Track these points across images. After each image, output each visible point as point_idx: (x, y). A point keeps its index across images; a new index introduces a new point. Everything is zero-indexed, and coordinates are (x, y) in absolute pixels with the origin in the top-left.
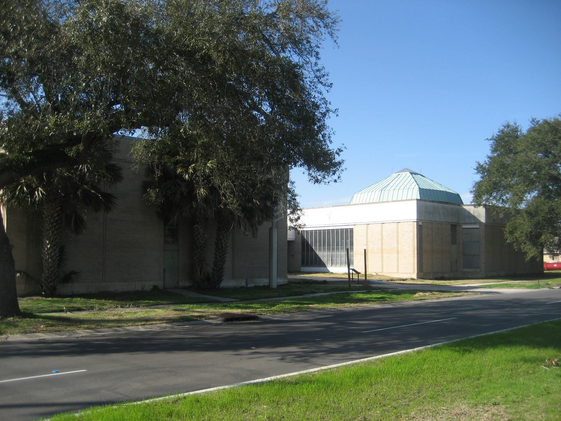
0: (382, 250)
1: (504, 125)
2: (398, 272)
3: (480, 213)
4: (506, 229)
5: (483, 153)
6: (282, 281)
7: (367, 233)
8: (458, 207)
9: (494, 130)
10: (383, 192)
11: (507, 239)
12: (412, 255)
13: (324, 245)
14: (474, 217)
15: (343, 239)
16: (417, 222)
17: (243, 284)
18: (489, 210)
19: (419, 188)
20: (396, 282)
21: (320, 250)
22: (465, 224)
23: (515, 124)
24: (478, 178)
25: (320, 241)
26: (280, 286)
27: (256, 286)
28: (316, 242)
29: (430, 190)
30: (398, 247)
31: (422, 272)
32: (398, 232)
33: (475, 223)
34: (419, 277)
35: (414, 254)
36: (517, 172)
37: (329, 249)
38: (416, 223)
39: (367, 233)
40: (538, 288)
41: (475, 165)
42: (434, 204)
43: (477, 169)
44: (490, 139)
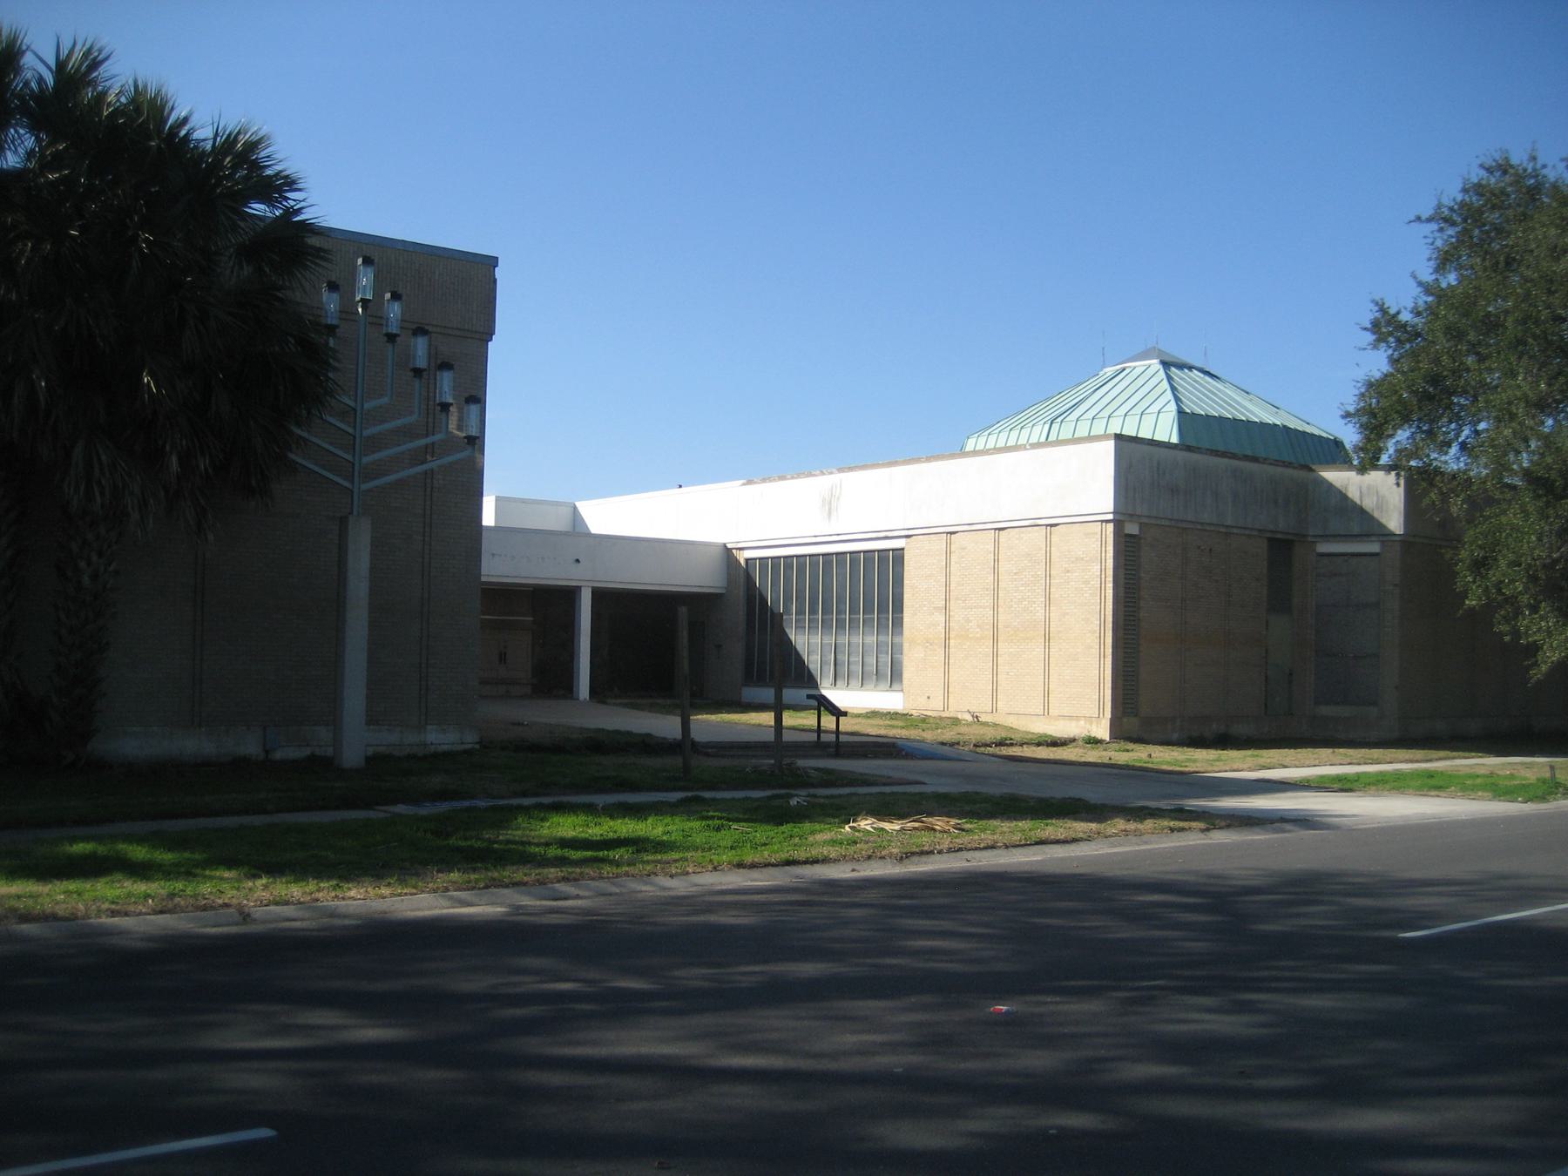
0: (995, 627)
1: (1489, 162)
2: (1046, 712)
3: (1380, 494)
4: (1464, 554)
5: (1405, 272)
6: (389, 739)
7: (948, 565)
8: (1302, 474)
9: (1449, 176)
10: (1056, 426)
11: (1464, 595)
12: (1095, 651)
13: (813, 611)
14: (1361, 511)
15: (867, 586)
16: (1118, 524)
17: (250, 746)
18: (1421, 484)
19: (1181, 412)
20: (1027, 752)
21: (800, 626)
22: (1327, 537)
23: (1534, 159)
24: (1377, 363)
25: (801, 598)
26: (377, 762)
27: (312, 759)
28: (788, 599)
29: (1221, 419)
30: (1047, 621)
31: (1134, 710)
32: (1049, 561)
33: (1363, 536)
34: (1120, 732)
35: (1102, 644)
36: (1510, 322)
37: (826, 625)
38: (1111, 527)
39: (948, 565)
40: (1543, 798)
41: (1368, 315)
42: (1195, 457)
43: (1375, 326)
44: (1429, 220)
